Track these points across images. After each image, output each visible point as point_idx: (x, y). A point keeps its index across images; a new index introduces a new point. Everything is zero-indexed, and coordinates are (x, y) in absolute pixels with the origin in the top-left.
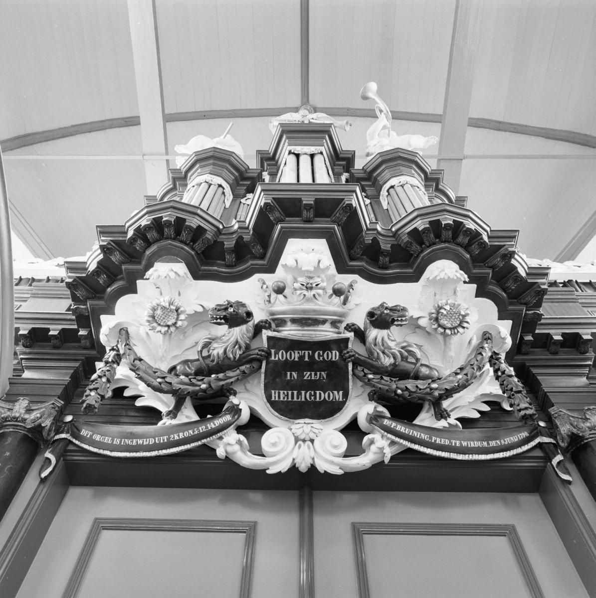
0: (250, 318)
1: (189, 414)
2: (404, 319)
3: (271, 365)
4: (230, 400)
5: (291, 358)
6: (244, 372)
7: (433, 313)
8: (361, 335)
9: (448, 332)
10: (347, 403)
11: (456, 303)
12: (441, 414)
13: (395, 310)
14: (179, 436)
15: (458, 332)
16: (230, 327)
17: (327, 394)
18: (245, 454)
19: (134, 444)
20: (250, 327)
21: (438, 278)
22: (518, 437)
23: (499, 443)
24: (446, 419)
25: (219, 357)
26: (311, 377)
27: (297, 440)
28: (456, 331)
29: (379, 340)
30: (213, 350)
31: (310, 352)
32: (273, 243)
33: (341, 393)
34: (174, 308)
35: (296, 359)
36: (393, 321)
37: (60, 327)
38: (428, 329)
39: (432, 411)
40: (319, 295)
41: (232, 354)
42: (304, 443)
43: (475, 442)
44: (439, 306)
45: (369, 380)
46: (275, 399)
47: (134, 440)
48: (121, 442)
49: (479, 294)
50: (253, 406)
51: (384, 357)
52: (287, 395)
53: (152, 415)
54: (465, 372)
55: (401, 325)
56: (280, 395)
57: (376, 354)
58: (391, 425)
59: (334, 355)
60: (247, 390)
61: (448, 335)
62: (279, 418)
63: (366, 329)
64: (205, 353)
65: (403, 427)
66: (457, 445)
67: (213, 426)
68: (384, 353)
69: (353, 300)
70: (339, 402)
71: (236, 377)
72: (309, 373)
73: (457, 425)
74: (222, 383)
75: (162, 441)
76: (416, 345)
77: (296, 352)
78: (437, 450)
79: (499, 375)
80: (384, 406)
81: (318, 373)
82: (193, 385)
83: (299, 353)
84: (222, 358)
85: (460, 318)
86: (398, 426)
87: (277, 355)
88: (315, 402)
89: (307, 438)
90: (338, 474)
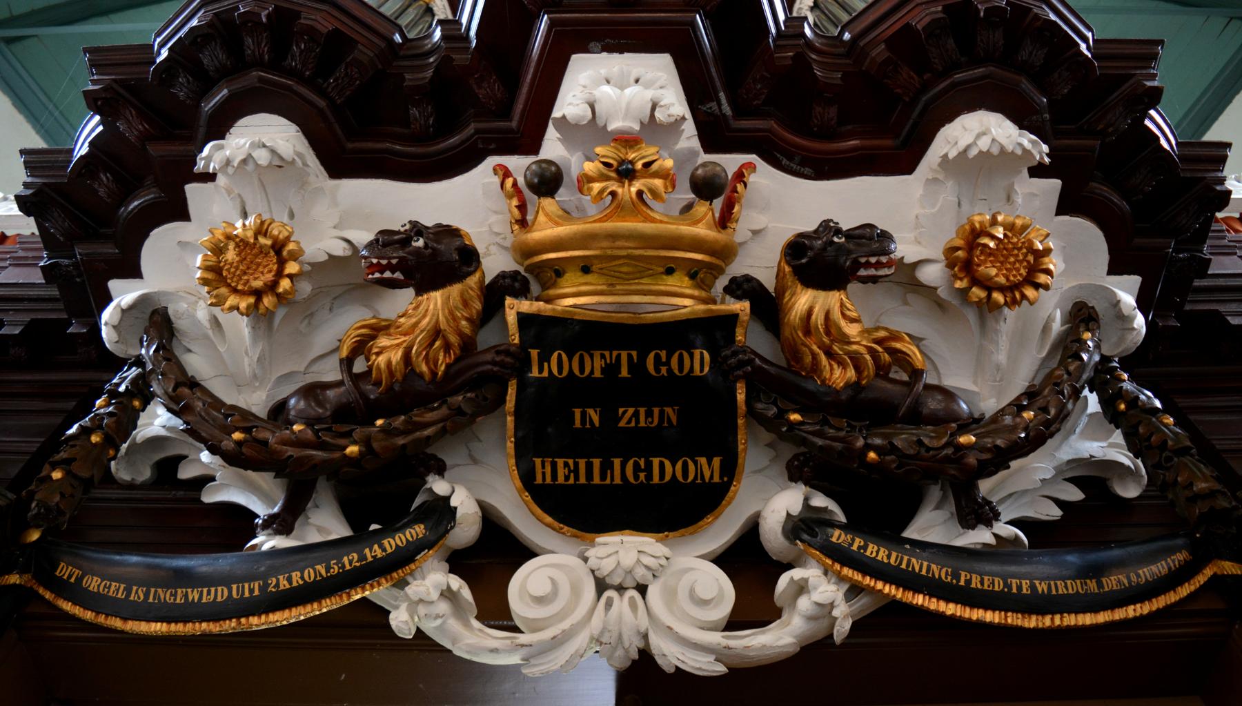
0: (470, 266)
1: (325, 523)
2: (884, 259)
3: (531, 390)
4: (428, 486)
5: (582, 370)
6: (459, 411)
7: (958, 249)
8: (768, 306)
9: (998, 297)
10: (732, 488)
11: (1019, 222)
12: (976, 513)
13: (861, 237)
14: (290, 580)
15: (1024, 297)
16: (419, 293)
17: (679, 465)
18: (467, 625)
19: (178, 601)
20: (471, 289)
21: (973, 152)
22: (1168, 564)
23: (1126, 582)
24: (988, 524)
25: (391, 372)
26: (638, 422)
27: (601, 586)
28: (1018, 295)
29: (818, 318)
30: (378, 354)
31: (634, 353)
32: (533, 65)
33: (716, 461)
34: (269, 242)
35: (598, 374)
36: (857, 265)
37: (27, 318)
38: (942, 293)
39: (951, 506)
40: (655, 194)
41: (427, 363)
42: (621, 595)
43: (1069, 582)
44: (973, 229)
45: (793, 425)
46: (544, 479)
47: (179, 591)
48: (147, 595)
49: (1065, 206)
50: (483, 498)
51: (831, 365)
52: (576, 471)
53: (235, 525)
54: (1040, 402)
55: (874, 280)
56: (558, 471)
57: (808, 359)
58: (851, 545)
59: (700, 361)
60: (475, 461)
61: (998, 307)
62: (554, 529)
63: (781, 288)
64: (359, 366)
65: (882, 549)
66: (1025, 591)
67: (379, 553)
68: (830, 354)
69: (748, 219)
70: (711, 485)
71: (440, 425)
72: (631, 411)
73: (1017, 537)
74: (401, 441)
75: (247, 594)
76: (908, 335)
77: (597, 354)
78: (973, 605)
79: (1118, 413)
80: (828, 494)
81: (656, 411)
82: (322, 446)
83: (603, 356)
84: (399, 376)
85: (1028, 262)
86: (871, 546)
87: (546, 365)
88: (647, 488)
89: (629, 583)
90: (705, 674)
